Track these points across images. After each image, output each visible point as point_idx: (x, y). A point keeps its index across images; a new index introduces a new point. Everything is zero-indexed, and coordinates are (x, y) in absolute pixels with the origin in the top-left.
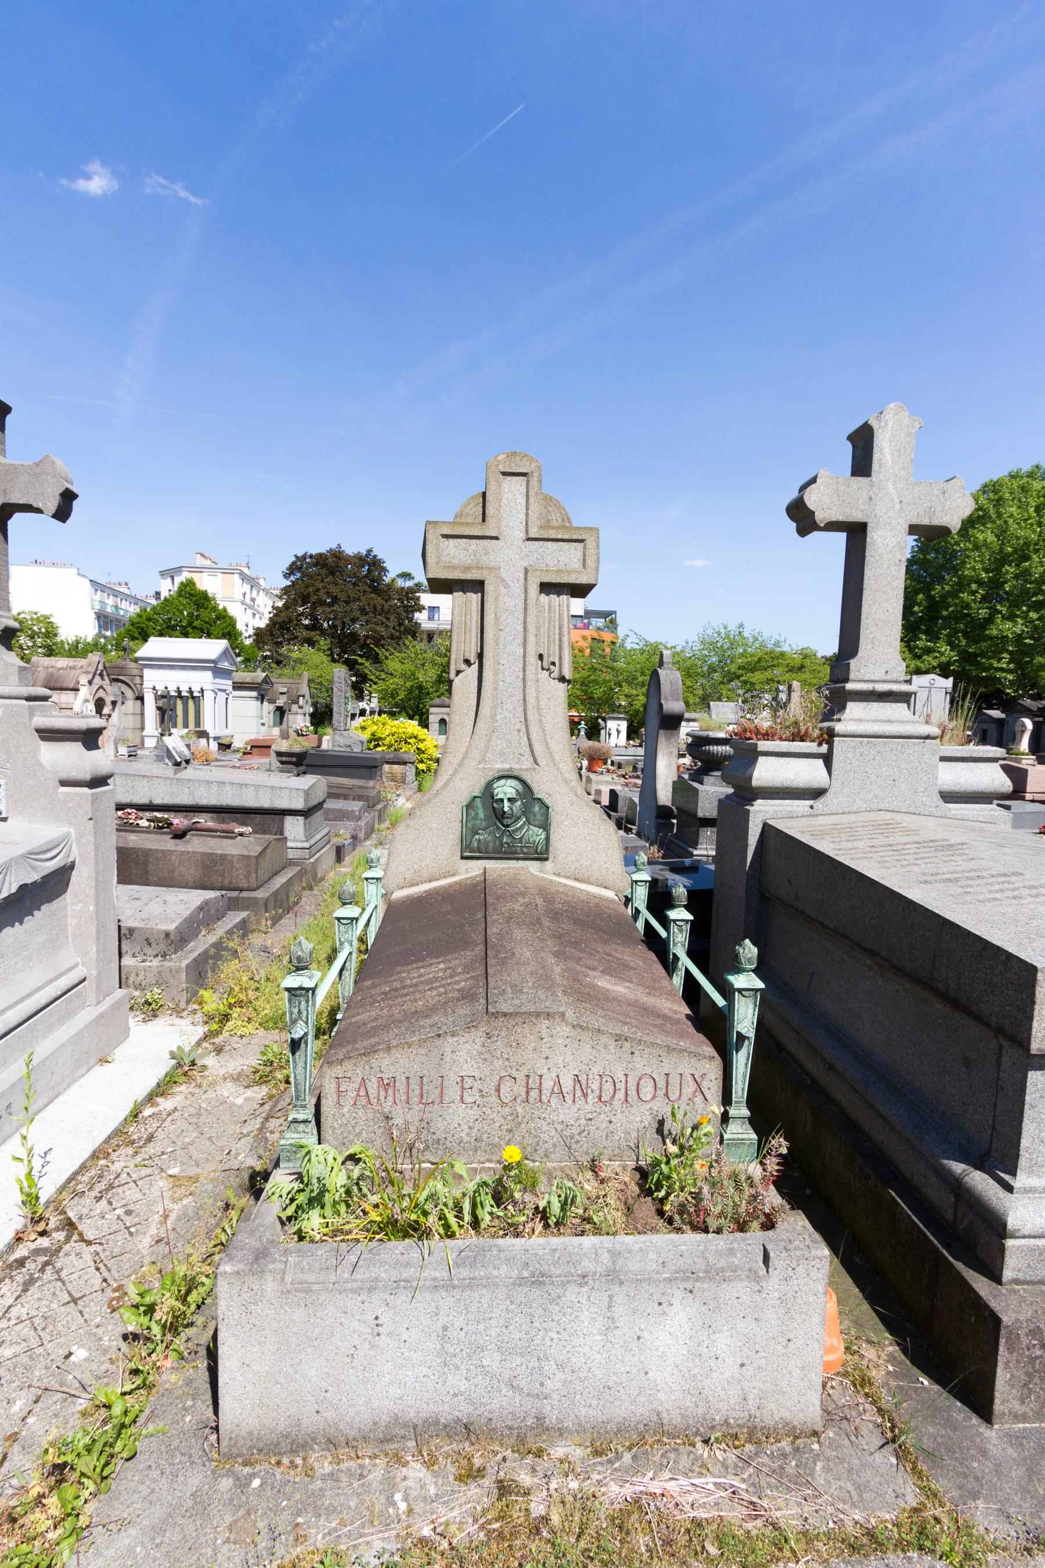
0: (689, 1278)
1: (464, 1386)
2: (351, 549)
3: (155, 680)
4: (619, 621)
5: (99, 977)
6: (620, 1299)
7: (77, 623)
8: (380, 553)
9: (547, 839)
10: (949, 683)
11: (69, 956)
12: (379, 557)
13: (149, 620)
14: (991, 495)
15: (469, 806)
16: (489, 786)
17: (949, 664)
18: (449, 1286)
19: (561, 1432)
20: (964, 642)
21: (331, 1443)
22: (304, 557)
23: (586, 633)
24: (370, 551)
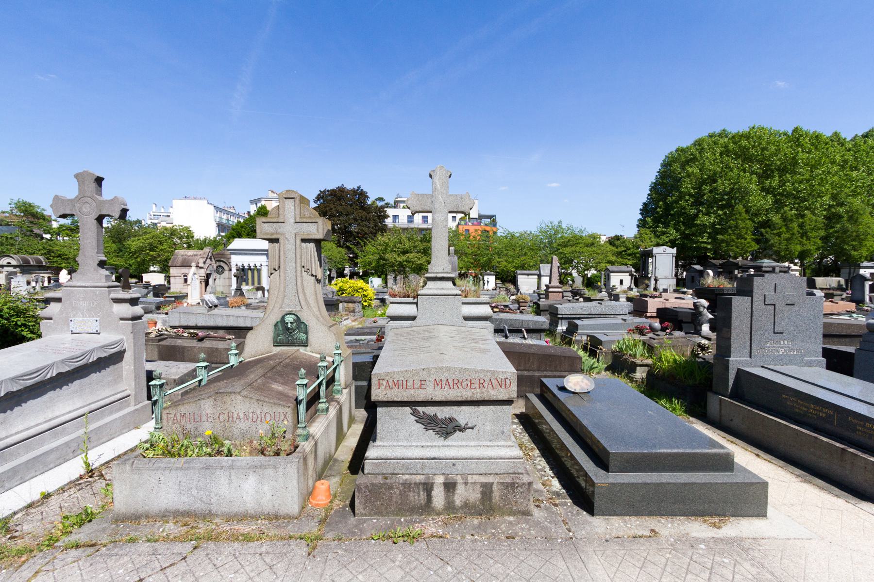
0: (255, 468)
1: (186, 500)
2: (350, 186)
3: (237, 261)
4: (497, 220)
5: (135, 395)
6: (233, 474)
7: (205, 228)
8: (365, 188)
9: (307, 338)
10: (674, 251)
11: (122, 386)
12: (365, 190)
13: (242, 227)
14: (697, 147)
15: (276, 325)
16: (283, 317)
17: (675, 240)
18: (181, 469)
19: (217, 515)
20: (683, 228)
21: (147, 517)
22: (325, 191)
23: (478, 227)
24: (359, 187)
